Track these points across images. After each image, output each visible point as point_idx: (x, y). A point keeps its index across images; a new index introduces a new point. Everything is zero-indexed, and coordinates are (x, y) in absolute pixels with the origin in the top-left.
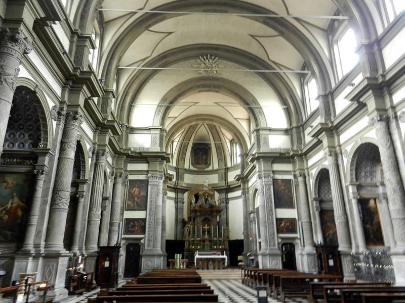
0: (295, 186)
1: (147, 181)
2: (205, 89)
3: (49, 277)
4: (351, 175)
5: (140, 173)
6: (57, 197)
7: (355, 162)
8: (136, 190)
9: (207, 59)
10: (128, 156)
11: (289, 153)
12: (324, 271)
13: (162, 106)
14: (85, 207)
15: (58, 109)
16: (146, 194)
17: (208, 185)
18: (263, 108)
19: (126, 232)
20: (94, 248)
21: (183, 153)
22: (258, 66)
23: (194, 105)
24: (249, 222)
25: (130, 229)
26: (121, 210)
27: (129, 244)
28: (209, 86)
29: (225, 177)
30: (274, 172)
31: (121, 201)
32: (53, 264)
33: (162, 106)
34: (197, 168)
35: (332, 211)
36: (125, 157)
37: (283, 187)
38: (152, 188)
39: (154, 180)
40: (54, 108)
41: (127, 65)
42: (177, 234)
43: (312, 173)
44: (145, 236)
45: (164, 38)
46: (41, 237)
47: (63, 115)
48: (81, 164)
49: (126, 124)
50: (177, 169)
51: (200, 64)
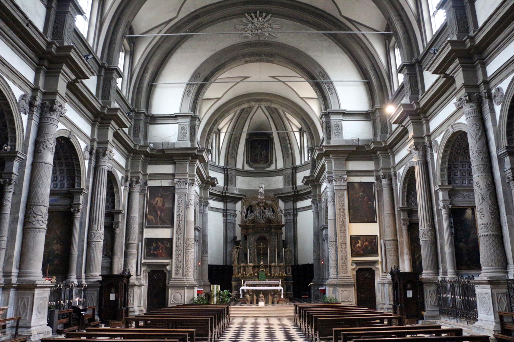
1: (175, 187)
2: (252, 58)
3: (24, 312)
4: (442, 176)
6: (30, 213)
7: (447, 158)
9: (256, 16)
10: (146, 154)
11: (369, 146)
12: (399, 305)
13: (194, 84)
14: (83, 224)
15: (28, 99)
16: (171, 206)
17: (265, 191)
18: (334, 83)
19: (148, 255)
20: (97, 275)
21: (233, 147)
22: (326, 24)
23: (241, 81)
24: (320, 241)
25: (152, 252)
27: (359, 269)
29: (293, 180)
30: (350, 173)
31: (139, 215)
32: (28, 297)
33: (194, 84)
34: (253, 168)
35: (418, 224)
36: (143, 156)
37: (361, 194)
38: (179, 198)
39: (183, 187)
40: (23, 97)
41: (144, 31)
42: (226, 257)
43: (399, 173)
44: (172, 261)
46: (12, 263)
47: (36, 106)
48: (76, 168)
49: (144, 110)
50: (225, 170)
51: (247, 24)
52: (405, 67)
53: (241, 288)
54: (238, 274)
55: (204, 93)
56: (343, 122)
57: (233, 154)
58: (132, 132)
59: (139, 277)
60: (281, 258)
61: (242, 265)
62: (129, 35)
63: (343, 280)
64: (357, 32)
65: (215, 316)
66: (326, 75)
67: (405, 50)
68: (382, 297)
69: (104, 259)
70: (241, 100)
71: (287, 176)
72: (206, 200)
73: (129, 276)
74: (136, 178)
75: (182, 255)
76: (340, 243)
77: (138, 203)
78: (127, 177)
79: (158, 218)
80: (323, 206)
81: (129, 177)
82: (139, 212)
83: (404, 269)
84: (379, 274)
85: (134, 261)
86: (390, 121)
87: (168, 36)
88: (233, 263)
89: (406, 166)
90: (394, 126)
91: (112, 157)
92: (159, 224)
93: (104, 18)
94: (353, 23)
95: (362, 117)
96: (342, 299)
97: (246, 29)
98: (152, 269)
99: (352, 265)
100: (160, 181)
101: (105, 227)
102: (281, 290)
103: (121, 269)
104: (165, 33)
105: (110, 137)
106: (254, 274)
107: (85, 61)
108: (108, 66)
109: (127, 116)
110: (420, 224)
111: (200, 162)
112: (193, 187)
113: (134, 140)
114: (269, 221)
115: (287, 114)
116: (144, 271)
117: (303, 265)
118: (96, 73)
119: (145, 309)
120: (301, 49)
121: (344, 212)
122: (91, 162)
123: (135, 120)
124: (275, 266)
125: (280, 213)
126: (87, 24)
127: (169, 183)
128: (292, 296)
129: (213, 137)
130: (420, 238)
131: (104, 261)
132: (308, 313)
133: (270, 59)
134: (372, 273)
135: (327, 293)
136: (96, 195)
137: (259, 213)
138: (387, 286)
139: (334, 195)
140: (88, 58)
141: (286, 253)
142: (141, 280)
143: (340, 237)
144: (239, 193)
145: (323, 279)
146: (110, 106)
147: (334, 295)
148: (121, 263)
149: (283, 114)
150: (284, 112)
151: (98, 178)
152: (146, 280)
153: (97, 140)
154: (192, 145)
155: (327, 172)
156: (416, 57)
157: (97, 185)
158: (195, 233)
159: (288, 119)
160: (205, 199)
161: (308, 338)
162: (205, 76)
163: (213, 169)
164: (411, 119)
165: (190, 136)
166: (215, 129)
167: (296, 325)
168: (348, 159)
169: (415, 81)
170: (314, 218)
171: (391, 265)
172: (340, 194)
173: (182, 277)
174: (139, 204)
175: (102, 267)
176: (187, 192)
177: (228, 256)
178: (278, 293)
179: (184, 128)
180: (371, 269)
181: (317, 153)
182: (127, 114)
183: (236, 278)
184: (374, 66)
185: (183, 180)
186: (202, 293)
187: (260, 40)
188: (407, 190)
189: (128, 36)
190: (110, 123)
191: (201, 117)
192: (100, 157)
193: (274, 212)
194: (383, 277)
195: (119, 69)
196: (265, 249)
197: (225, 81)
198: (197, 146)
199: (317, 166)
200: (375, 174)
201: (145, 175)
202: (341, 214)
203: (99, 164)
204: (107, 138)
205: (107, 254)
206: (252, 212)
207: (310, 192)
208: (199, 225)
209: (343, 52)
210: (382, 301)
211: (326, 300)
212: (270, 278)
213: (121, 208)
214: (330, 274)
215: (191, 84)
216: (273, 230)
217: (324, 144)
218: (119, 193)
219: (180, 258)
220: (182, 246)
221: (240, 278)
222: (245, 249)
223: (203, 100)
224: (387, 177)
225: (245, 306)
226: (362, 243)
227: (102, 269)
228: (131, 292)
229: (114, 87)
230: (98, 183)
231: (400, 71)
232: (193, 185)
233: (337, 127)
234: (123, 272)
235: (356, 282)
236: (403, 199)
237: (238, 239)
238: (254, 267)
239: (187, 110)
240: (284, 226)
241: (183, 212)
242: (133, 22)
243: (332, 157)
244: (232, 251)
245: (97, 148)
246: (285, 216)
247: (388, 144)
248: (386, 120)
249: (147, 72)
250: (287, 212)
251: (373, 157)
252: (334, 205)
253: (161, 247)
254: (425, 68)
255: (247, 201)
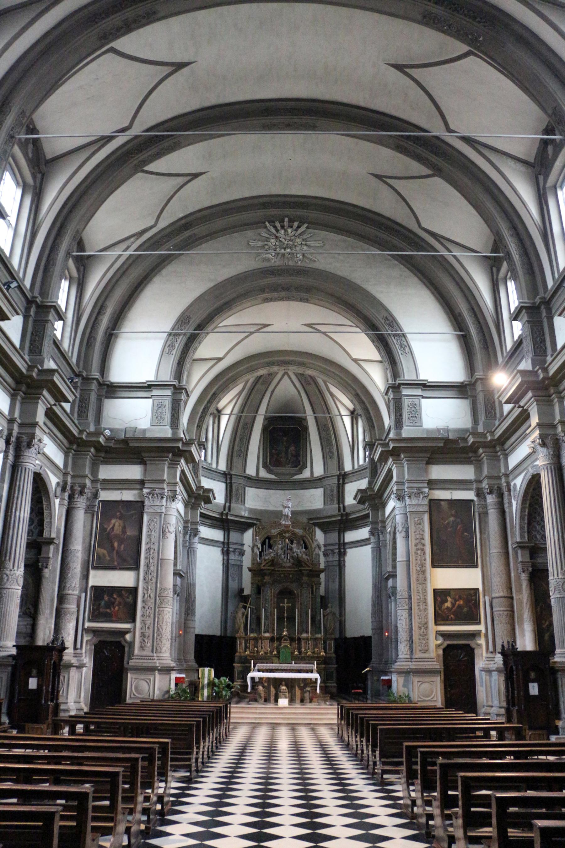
0: (479, 516)
1: (143, 502)
2: (275, 294)
5: (126, 486)
8: (116, 524)
9: (283, 227)
10: (99, 448)
11: (465, 440)
12: (516, 708)
13: (179, 335)
17: (293, 513)
18: (409, 336)
19: (96, 615)
21: (241, 440)
22: (396, 241)
23: (257, 331)
24: (384, 599)
25: (102, 610)
26: (82, 568)
27: (449, 646)
28: (287, 288)
30: (433, 484)
31: (84, 548)
33: (179, 335)
36: (92, 450)
37: (452, 519)
38: (150, 520)
39: (157, 502)
41: (102, 247)
43: (515, 484)
44: (135, 625)
45: (182, 187)
49: (96, 374)
51: (267, 240)
52: (524, 311)
53: (250, 675)
54: (246, 651)
55: (196, 349)
56: (423, 401)
57: (241, 450)
58: (76, 410)
59: (78, 651)
60: (318, 625)
61: (252, 635)
62: (77, 252)
63: (422, 663)
64: (446, 253)
65: (204, 719)
66: (395, 324)
67: (523, 284)
68: (486, 693)
69: (21, 619)
70: (256, 362)
71: (329, 489)
72: (194, 527)
73: (63, 648)
74: (79, 486)
75: (152, 616)
76: (416, 601)
77: (82, 527)
78: (65, 483)
79: (115, 552)
80: (389, 538)
81: (69, 483)
82: (84, 542)
83: (525, 646)
84: (482, 654)
85: (71, 624)
86: (500, 399)
87: (141, 255)
88: (237, 631)
89: (526, 473)
90: (507, 408)
91: (43, 449)
92: (116, 563)
93: (39, 224)
94: (440, 239)
95: (454, 392)
96: (418, 696)
97: (266, 247)
98: (100, 639)
99: (436, 639)
100: (120, 491)
101: (26, 566)
102: (316, 679)
103: (49, 637)
104: (135, 251)
105: (41, 417)
106: (271, 652)
107: (5, 291)
108: (42, 302)
109: (69, 383)
110: (550, 570)
111: (187, 463)
112: (174, 503)
113: (79, 423)
114: (298, 562)
115: (330, 386)
116: (87, 641)
117: (355, 639)
118: (22, 313)
119: (86, 705)
120: (354, 281)
121: (423, 550)
122: (7, 456)
123: (81, 390)
124: (307, 639)
125: (317, 550)
126: (11, 233)
127: (135, 495)
128: (334, 690)
129: (209, 420)
130: (551, 594)
131: (21, 623)
132: (362, 719)
133: (304, 295)
134: (470, 652)
135: (394, 685)
136: (14, 511)
137: (282, 549)
138: (495, 675)
139: (407, 520)
140: (10, 287)
141: (326, 618)
142: (82, 657)
143: (416, 592)
144: (249, 516)
145: (386, 663)
146: (42, 366)
147: (406, 689)
148: (50, 627)
149: (325, 387)
150: (325, 382)
151: (18, 483)
152: (90, 658)
153: (19, 421)
154: (174, 433)
155: (396, 482)
156: (542, 294)
157: (16, 495)
158: (175, 581)
159: (332, 395)
160: (192, 523)
161: (362, 760)
162: (198, 321)
163: (207, 474)
164: (534, 396)
165: (171, 419)
166: (212, 409)
167: (341, 739)
168: (430, 461)
169: (540, 334)
170: (374, 559)
171: (502, 639)
172: (416, 519)
173: (151, 654)
174: (84, 530)
175: (18, 633)
176: (164, 510)
177: (228, 621)
178: (312, 685)
179: (162, 405)
180: (468, 645)
181: (379, 450)
182: (69, 379)
183: (241, 657)
184: (473, 309)
185: (158, 491)
186: (183, 682)
187: (288, 266)
188: (528, 513)
189: (75, 254)
190: (41, 394)
191: (190, 388)
192: (23, 449)
193: (306, 548)
194: (490, 659)
195: (59, 306)
196: (292, 610)
197: (230, 331)
198: (182, 436)
199: (379, 472)
200: (474, 486)
201: (95, 481)
202: (419, 552)
203: (20, 460)
204: (35, 418)
205: (27, 611)
206: (270, 547)
207: (367, 516)
208: (182, 567)
209: (424, 286)
210: (487, 702)
211: (392, 698)
212: (300, 659)
213: (53, 535)
214: (400, 653)
215: (175, 335)
216: (305, 579)
217: (391, 435)
218: (51, 510)
219: (149, 622)
220: (153, 601)
221: (248, 658)
222: (258, 610)
223: (194, 360)
224: (495, 491)
225: (255, 705)
226: (453, 602)
227: (17, 637)
228: (64, 677)
229: (50, 336)
230: (17, 492)
231: (515, 317)
232: (173, 500)
233: (413, 409)
234: (53, 642)
235: (442, 667)
236: (521, 528)
237: (247, 592)
238: (272, 639)
239: (167, 376)
240: (323, 572)
241: (157, 544)
242: (85, 232)
243: (405, 457)
244: (235, 612)
245: (18, 433)
246: (325, 555)
247: (496, 437)
248: (493, 397)
249: (105, 313)
250: (328, 548)
251: (472, 458)
252: (407, 537)
253: (117, 603)
254: (556, 311)
255: (263, 529)
